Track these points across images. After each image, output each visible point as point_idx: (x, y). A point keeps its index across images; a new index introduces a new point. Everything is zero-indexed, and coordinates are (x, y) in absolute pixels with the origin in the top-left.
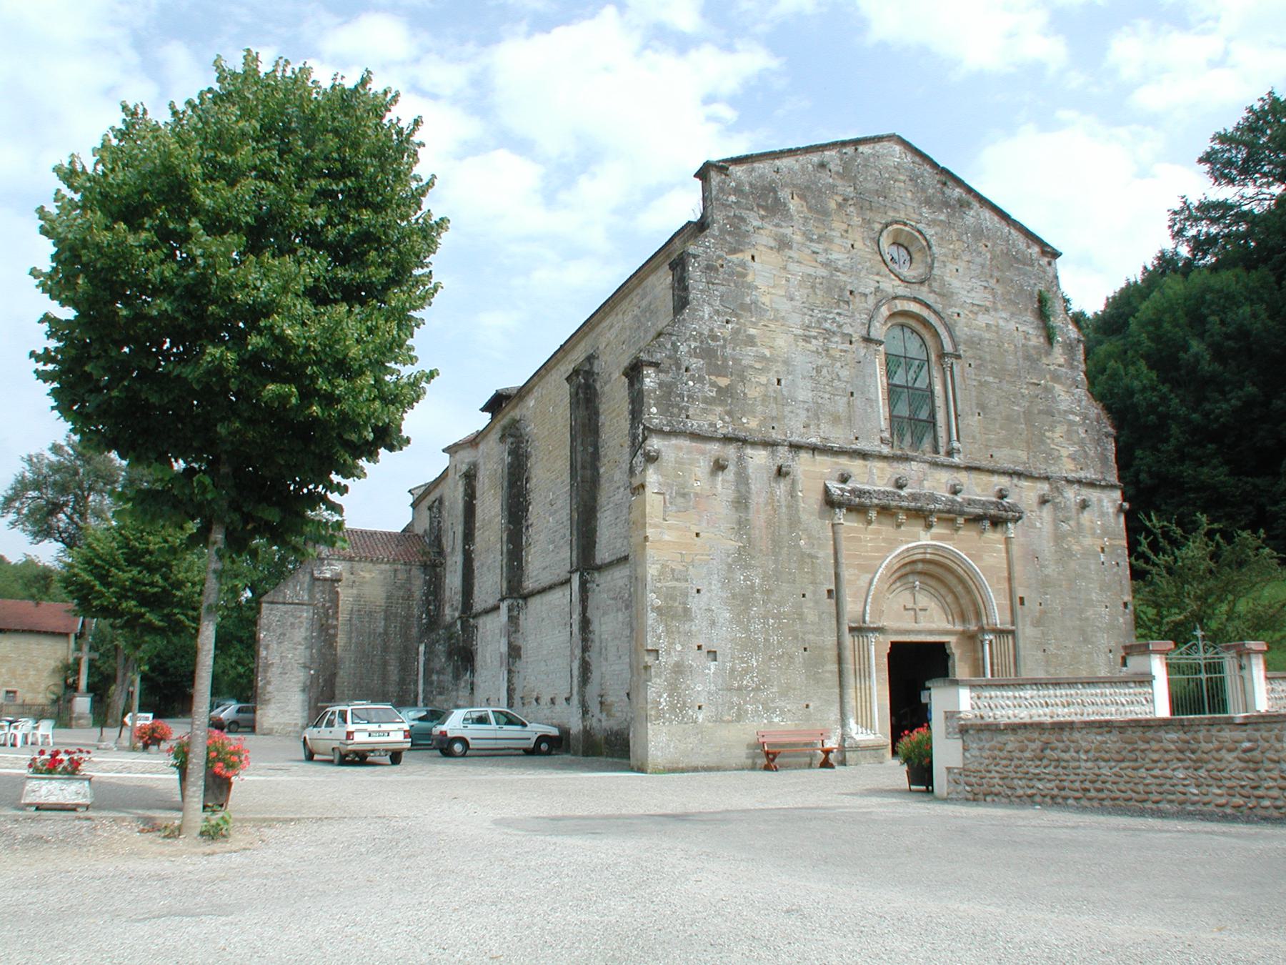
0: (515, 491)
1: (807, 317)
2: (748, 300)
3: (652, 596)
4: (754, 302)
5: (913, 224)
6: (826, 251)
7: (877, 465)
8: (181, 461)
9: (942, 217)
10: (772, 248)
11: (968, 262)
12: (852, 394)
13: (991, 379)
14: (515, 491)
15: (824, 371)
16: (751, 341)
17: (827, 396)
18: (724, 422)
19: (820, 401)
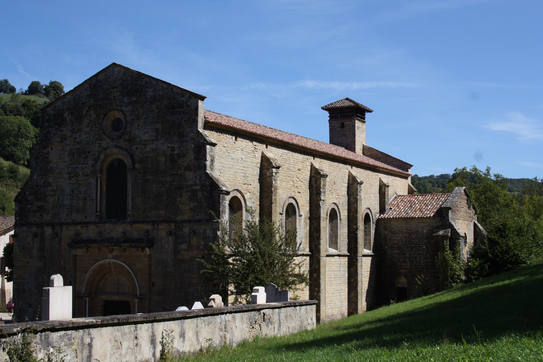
0: (429, 186)
1: (70, 169)
2: (49, 168)
3: (144, 320)
4: (51, 168)
5: (119, 108)
6: (80, 136)
7: (92, 227)
8: (135, 301)
9: (134, 99)
10: (59, 142)
11: (145, 118)
12: (86, 199)
13: (150, 177)
14: (429, 186)
15: (75, 191)
16: (49, 185)
17: (75, 201)
18: (39, 219)
19: (73, 204)
